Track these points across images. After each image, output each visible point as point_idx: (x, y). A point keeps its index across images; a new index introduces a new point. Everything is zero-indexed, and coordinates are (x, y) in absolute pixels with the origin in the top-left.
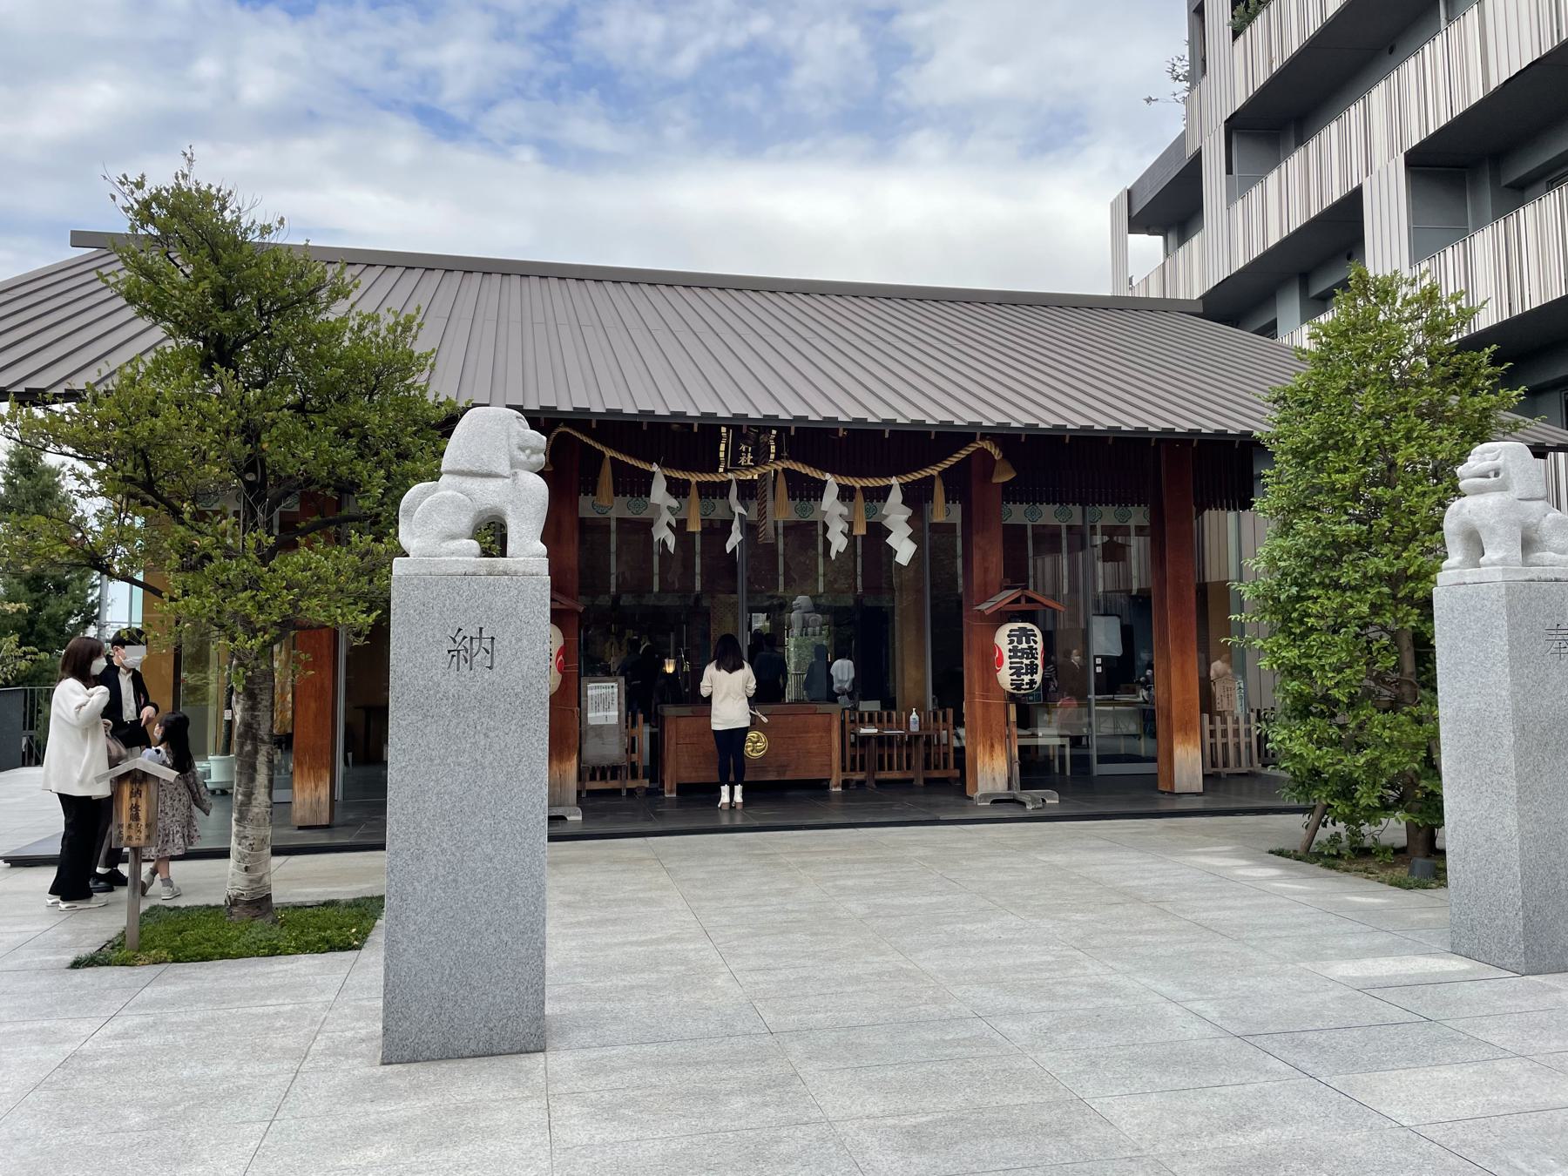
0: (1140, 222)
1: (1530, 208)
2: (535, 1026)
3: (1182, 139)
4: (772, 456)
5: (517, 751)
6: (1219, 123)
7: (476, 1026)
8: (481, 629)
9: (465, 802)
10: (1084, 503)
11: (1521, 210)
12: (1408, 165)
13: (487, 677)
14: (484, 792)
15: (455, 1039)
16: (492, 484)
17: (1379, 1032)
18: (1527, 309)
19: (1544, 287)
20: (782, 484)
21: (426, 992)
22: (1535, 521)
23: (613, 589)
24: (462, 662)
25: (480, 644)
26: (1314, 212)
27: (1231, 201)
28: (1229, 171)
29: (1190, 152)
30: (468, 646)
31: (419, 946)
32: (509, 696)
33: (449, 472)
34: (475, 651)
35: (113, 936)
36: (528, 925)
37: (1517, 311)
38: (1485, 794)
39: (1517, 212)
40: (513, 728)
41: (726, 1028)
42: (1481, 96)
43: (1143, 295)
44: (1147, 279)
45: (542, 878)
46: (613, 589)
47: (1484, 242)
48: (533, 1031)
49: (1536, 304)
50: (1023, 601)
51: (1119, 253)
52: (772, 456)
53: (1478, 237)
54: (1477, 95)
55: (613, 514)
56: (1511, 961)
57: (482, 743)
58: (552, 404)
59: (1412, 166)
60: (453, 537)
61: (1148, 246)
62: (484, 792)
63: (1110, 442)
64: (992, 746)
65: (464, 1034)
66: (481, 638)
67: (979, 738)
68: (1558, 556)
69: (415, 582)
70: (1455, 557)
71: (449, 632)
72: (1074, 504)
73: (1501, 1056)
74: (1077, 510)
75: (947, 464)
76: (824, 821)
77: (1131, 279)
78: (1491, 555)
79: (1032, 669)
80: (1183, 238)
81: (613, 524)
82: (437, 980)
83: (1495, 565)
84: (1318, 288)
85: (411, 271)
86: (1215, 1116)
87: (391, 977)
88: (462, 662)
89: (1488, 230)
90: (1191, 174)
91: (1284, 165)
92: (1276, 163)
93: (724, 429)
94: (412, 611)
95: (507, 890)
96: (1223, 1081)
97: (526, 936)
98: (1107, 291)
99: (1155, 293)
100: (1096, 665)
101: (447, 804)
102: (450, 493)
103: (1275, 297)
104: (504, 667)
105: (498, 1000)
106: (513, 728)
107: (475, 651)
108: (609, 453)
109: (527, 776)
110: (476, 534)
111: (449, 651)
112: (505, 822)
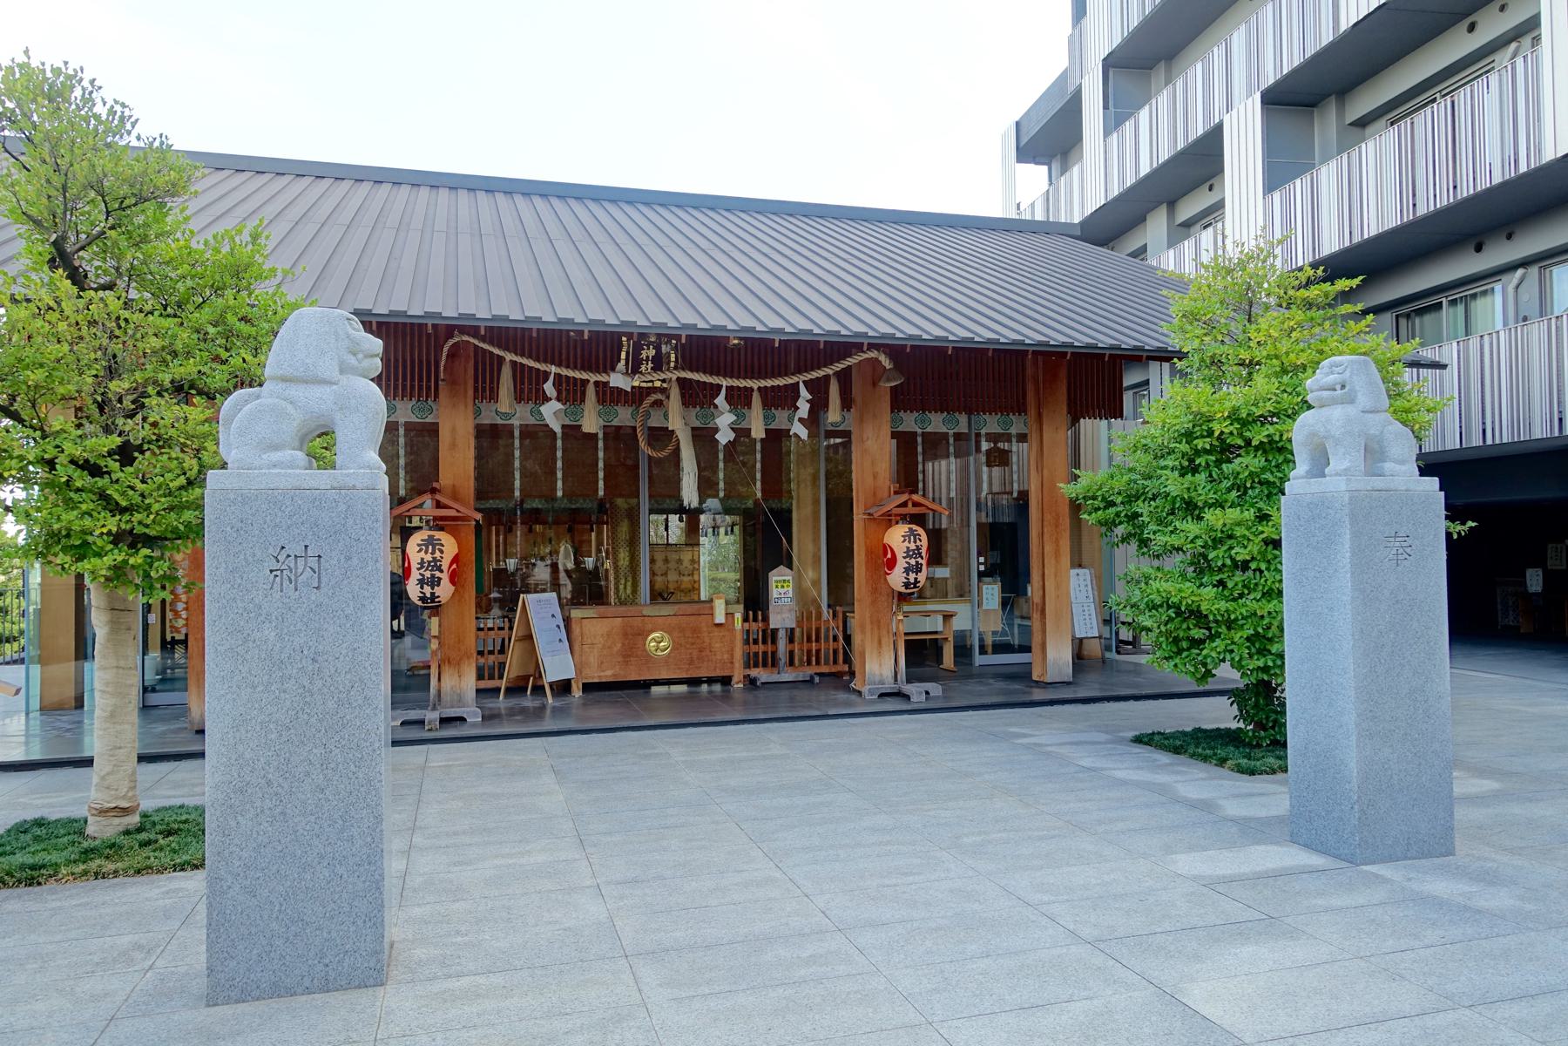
0: (1026, 152)
1: (1371, 144)
2: (374, 959)
3: (1063, 77)
4: (672, 364)
5: (348, 676)
6: (1097, 59)
7: (310, 962)
8: (306, 547)
9: (292, 731)
10: (969, 412)
11: (1363, 145)
12: (1263, 102)
13: (313, 598)
14: (313, 720)
15: (287, 976)
16: (317, 392)
17: (1223, 933)
18: (1366, 236)
19: (1380, 216)
20: (675, 393)
21: (253, 930)
22: (1377, 433)
23: (517, 494)
24: (286, 583)
25: (306, 565)
26: (1180, 145)
27: (1107, 133)
28: (1106, 107)
29: (1071, 89)
30: (292, 565)
31: (245, 882)
32: (339, 618)
33: (273, 378)
34: (300, 571)
35: (53, 818)
36: (365, 857)
37: (1357, 239)
38: (1324, 694)
39: (1360, 147)
40: (344, 652)
41: (581, 952)
42: (1331, 39)
43: (1029, 217)
44: (1033, 205)
45: (379, 808)
46: (517, 494)
47: (1328, 175)
48: (372, 965)
49: (1373, 233)
50: (910, 504)
51: (1009, 183)
52: (672, 364)
53: (1324, 169)
54: (1327, 37)
55: (516, 422)
56: (1346, 851)
57: (310, 668)
58: (403, 308)
59: (1268, 104)
60: (276, 448)
61: (1034, 177)
62: (313, 720)
63: (990, 354)
64: (880, 642)
65: (296, 972)
66: (306, 557)
67: (868, 634)
68: (1398, 467)
69: (232, 496)
70: (1302, 466)
71: (271, 550)
72: (960, 413)
73: (1339, 958)
74: (963, 419)
75: (769, 383)
76: (718, 718)
77: (1018, 205)
78: (1336, 464)
79: (917, 567)
80: (1065, 169)
81: (517, 433)
82: (266, 917)
83: (1340, 475)
84: (1187, 210)
85: (340, 181)
86: (1061, 1037)
87: (215, 916)
88: (286, 583)
89: (1333, 164)
90: (1072, 108)
91: (1154, 101)
92: (1146, 99)
93: (624, 339)
94: (228, 529)
95: (341, 822)
96: (1071, 995)
97: (362, 869)
98: (997, 212)
99: (1039, 216)
100: (979, 564)
101: (272, 733)
102: (270, 401)
103: (1145, 220)
104: (333, 587)
105: (334, 934)
106: (344, 652)
107: (300, 571)
108: (509, 357)
109: (360, 702)
110: (303, 441)
111: (271, 571)
112: (337, 751)
